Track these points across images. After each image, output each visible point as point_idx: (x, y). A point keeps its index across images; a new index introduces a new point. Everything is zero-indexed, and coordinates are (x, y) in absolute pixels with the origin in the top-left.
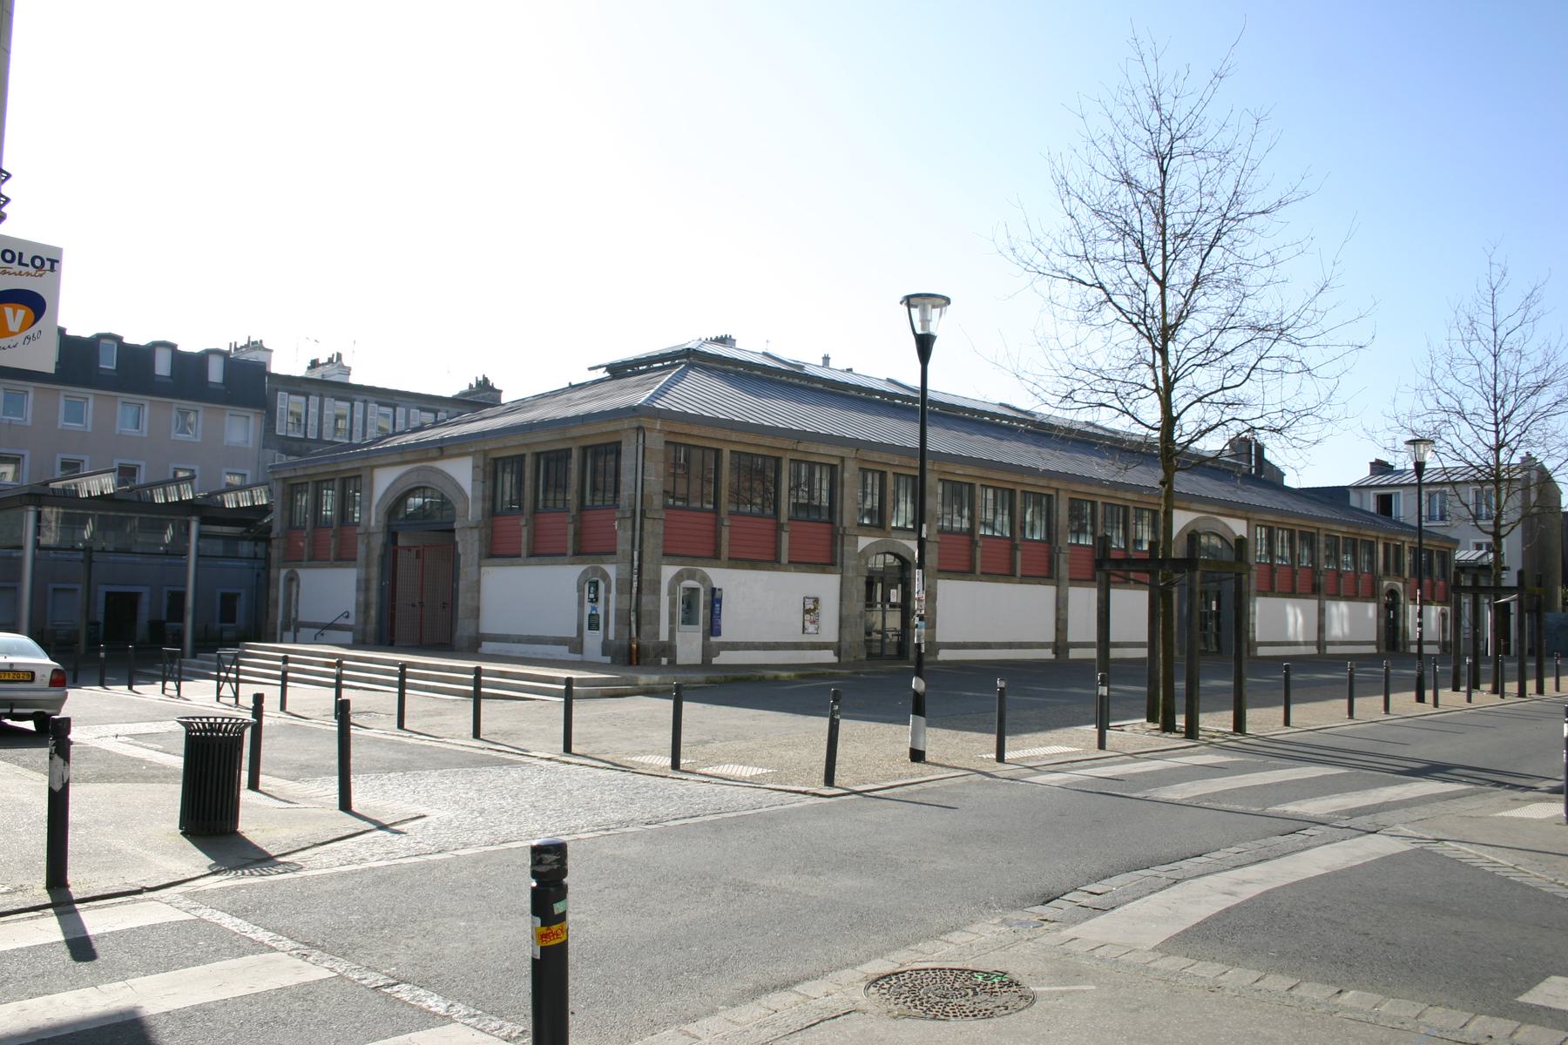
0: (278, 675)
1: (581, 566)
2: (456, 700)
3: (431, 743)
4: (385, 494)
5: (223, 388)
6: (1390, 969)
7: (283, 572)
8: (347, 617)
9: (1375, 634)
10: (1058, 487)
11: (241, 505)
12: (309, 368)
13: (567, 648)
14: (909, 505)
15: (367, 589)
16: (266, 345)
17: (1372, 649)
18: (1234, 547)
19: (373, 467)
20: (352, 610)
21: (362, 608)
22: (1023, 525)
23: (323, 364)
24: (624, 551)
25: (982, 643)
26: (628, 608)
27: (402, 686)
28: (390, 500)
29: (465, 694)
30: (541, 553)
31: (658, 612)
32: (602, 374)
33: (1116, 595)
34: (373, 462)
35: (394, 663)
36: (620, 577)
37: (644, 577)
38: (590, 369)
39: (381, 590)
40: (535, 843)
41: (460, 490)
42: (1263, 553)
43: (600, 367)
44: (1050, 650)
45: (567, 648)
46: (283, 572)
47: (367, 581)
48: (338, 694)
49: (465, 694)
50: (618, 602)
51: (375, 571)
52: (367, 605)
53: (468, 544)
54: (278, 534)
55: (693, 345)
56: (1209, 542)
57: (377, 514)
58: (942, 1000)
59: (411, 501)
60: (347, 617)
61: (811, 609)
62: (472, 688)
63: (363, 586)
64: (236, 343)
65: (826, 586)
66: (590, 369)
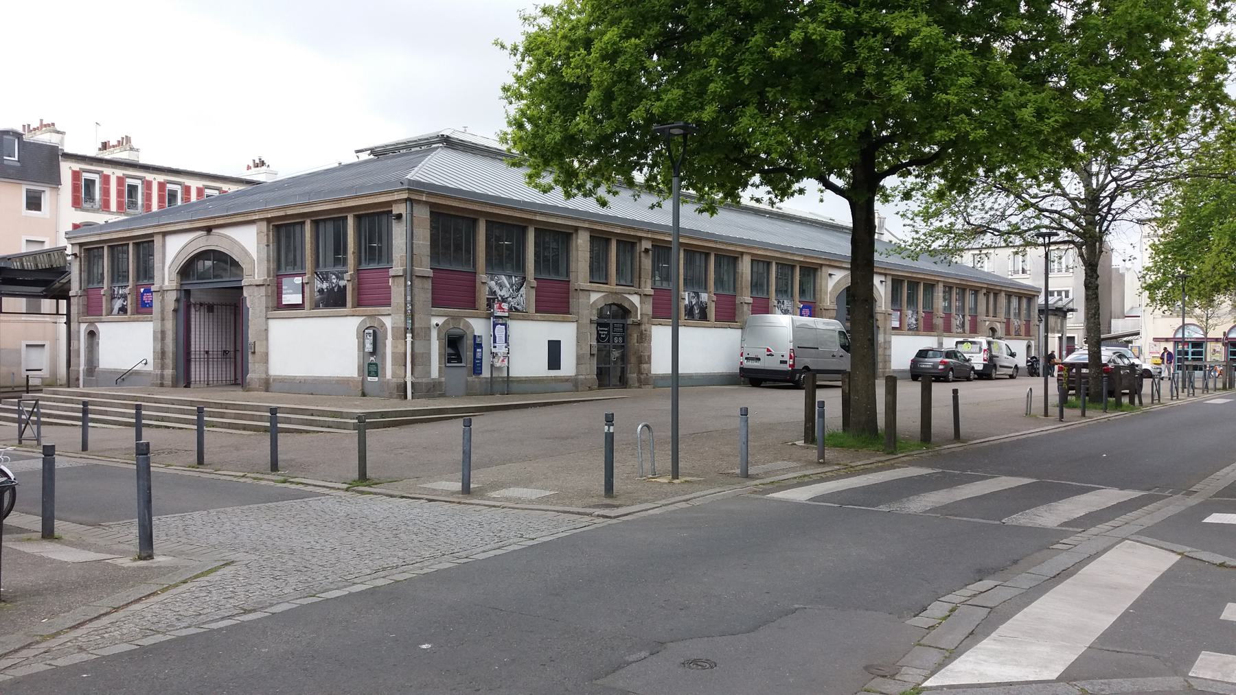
0: (15, 418)
2: (250, 435)
3: (188, 473)
5: (19, 164)
6: (164, 658)
7: (83, 327)
8: (146, 364)
11: (40, 268)
12: (100, 149)
15: (163, 339)
16: (706, 215)
20: (151, 361)
23: (114, 146)
24: (398, 303)
26: (403, 350)
27: (85, 419)
28: (182, 260)
29: (265, 429)
31: (429, 354)
32: (365, 156)
35: (192, 403)
36: (396, 325)
37: (416, 326)
39: (176, 339)
40: (151, 561)
41: (247, 253)
43: (366, 150)
46: (83, 327)
47: (163, 333)
48: (139, 436)
49: (265, 429)
50: (394, 347)
51: (170, 325)
52: (163, 353)
53: (254, 301)
54: (77, 292)
55: (446, 133)
57: (170, 274)
59: (200, 263)
60: (146, 364)
61: (554, 349)
62: (196, 418)
63: (161, 336)
64: (29, 125)
65: (566, 332)
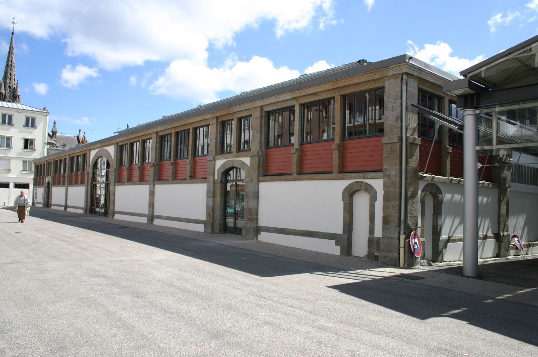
1: (249, 164)
4: (93, 159)
9: (39, 202)
10: (156, 131)
13: (334, 241)
14: (148, 146)
17: (81, 212)
18: (490, 113)
19: (90, 150)
21: (211, 195)
22: (366, 101)
25: (79, 207)
28: (94, 162)
30: (76, 183)
33: (484, 198)
34: (90, 148)
38: (4, 202)
42: (499, 135)
44: (63, 208)
45: (334, 241)
56: (189, 164)
58: (131, 310)
66: (4, 202)
